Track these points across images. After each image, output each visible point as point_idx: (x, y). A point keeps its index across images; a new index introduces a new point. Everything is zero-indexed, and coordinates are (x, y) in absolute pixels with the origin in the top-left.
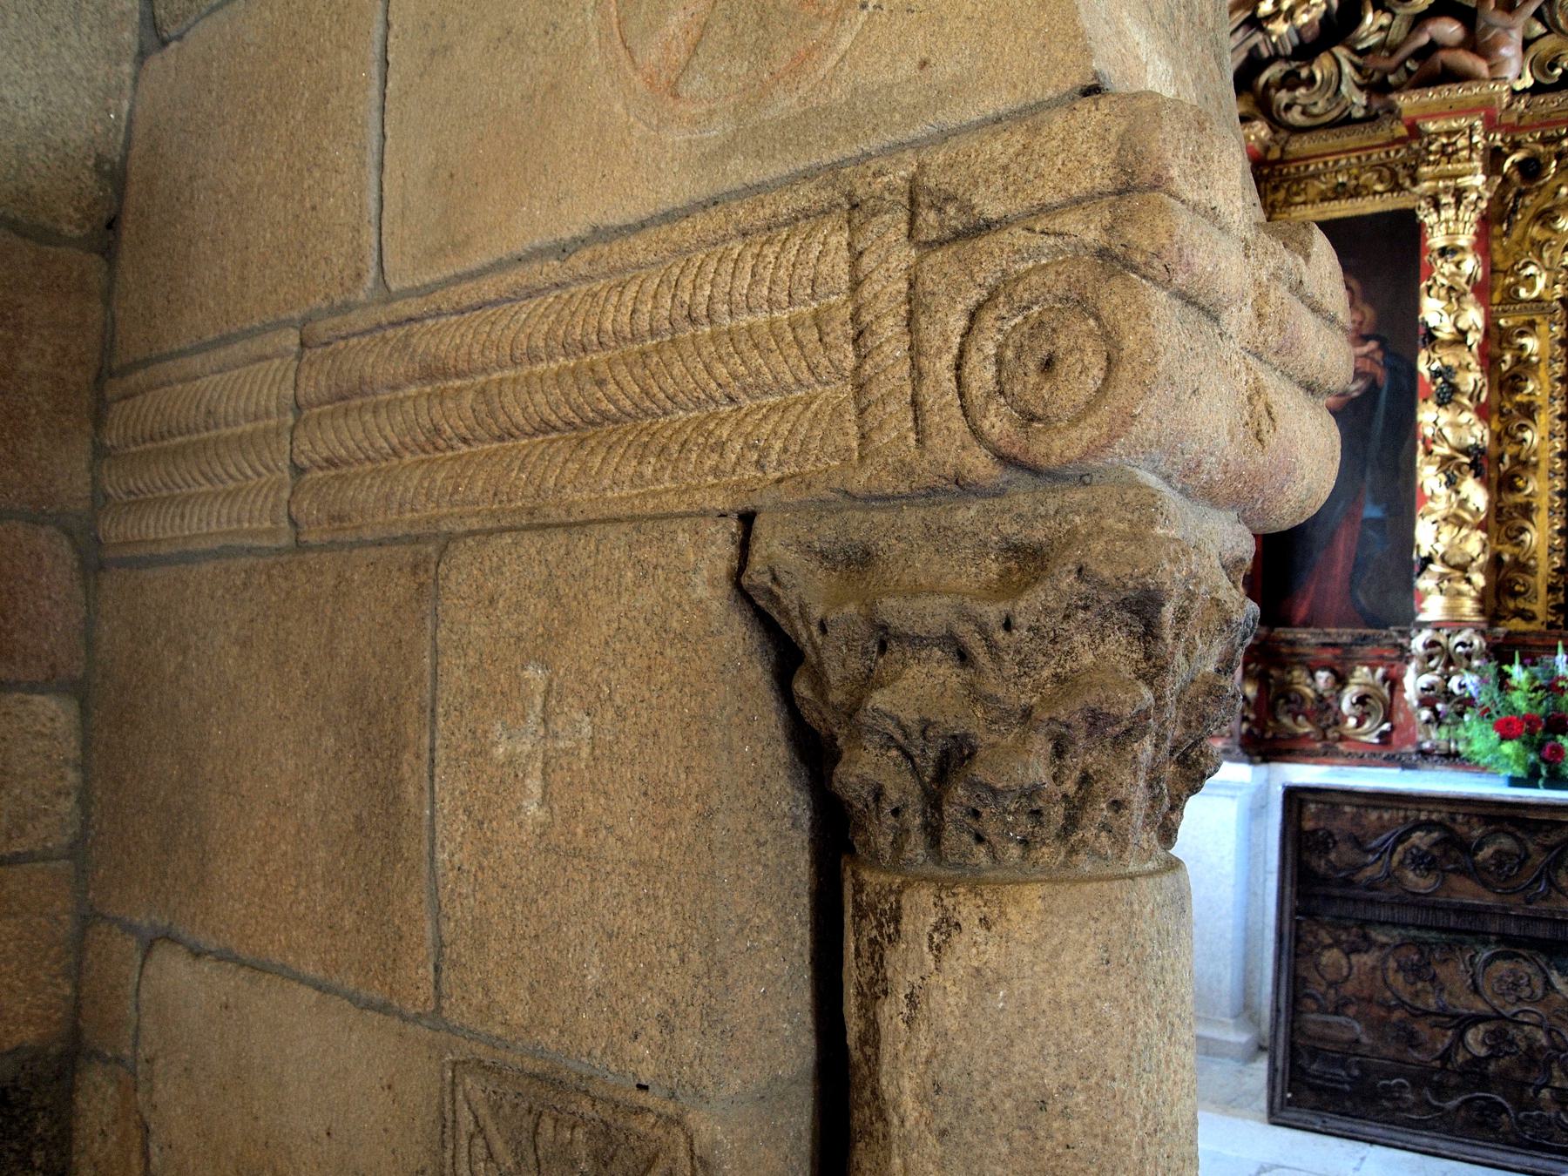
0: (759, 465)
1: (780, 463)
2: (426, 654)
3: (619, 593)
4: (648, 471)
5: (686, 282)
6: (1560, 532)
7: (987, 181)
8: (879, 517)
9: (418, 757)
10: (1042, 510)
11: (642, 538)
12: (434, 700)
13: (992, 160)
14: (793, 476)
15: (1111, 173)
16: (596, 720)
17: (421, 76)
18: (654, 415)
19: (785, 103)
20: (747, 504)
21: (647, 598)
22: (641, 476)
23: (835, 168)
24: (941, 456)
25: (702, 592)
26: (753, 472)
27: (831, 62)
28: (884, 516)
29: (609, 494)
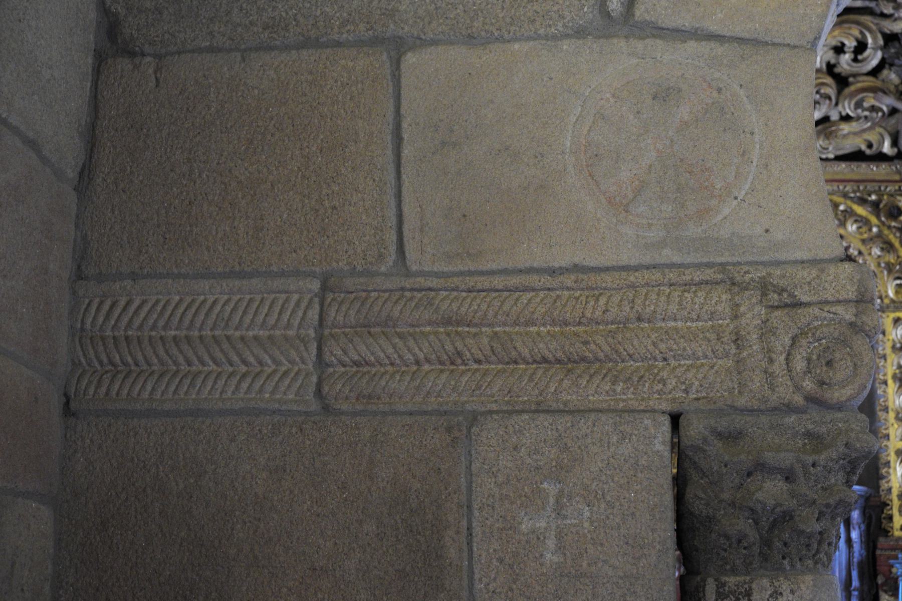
0: (686, 391)
1: (697, 391)
2: (462, 476)
3: (609, 447)
4: (619, 389)
5: (639, 301)
6: (883, 477)
7: (801, 286)
8: (748, 419)
9: (458, 533)
10: (824, 420)
11: (623, 421)
12: (469, 500)
13: (803, 278)
14: (703, 398)
15: (855, 294)
16: (595, 509)
17: (433, 153)
18: (616, 362)
19: (693, 230)
20: (675, 408)
21: (626, 449)
22: (614, 391)
23: (722, 265)
24: (783, 395)
25: (659, 447)
26: (680, 394)
27: (720, 217)
28: (751, 418)
29: (591, 398)
